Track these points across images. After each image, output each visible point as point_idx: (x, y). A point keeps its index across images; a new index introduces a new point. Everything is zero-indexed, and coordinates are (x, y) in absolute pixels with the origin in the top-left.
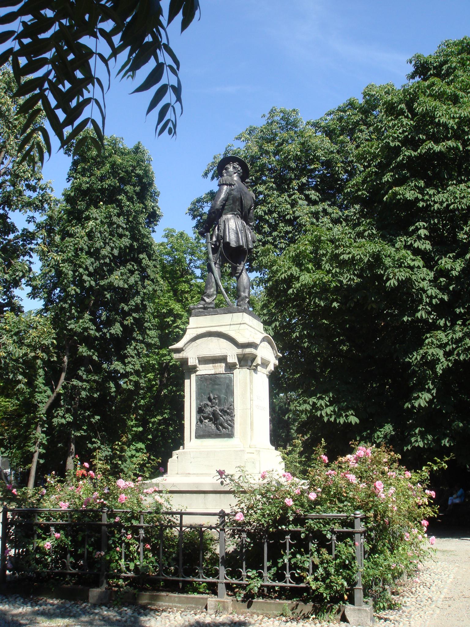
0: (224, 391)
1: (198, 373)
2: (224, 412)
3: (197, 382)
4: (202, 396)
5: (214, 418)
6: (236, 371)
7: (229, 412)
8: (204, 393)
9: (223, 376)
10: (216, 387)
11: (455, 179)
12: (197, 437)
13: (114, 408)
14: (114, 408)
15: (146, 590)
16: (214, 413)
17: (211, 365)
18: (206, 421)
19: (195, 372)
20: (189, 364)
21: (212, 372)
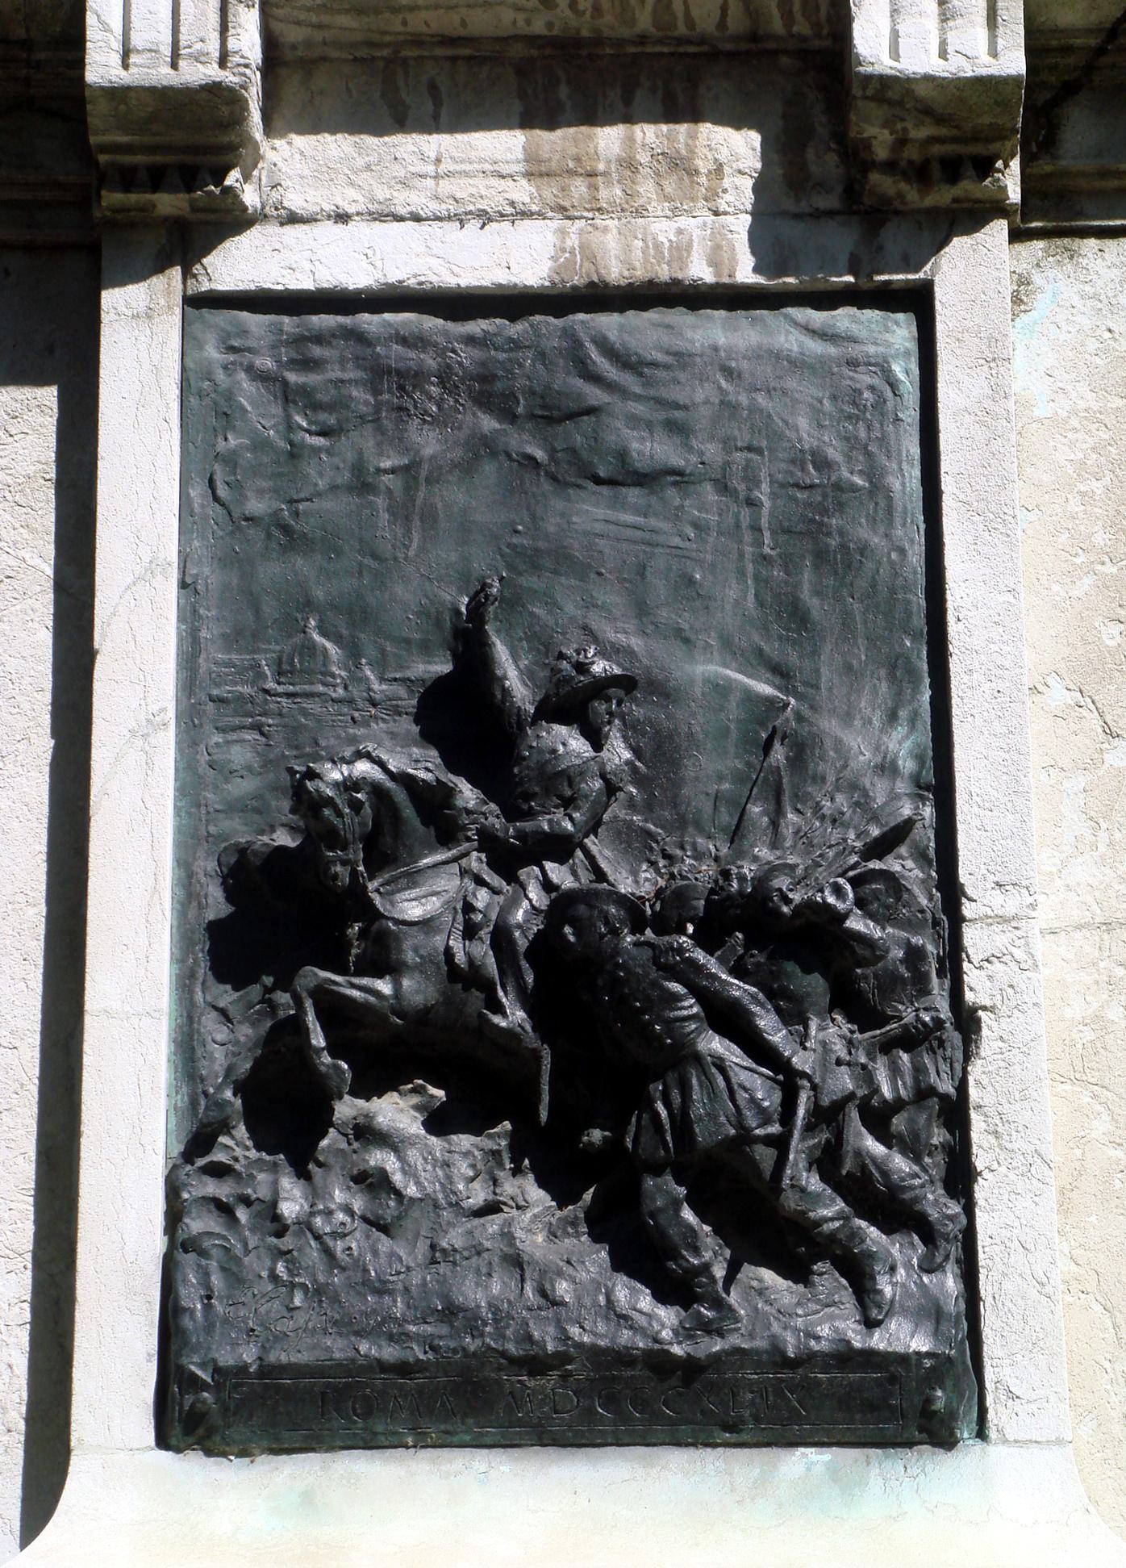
0: (735, 597)
1: (235, 265)
2: (798, 947)
3: (204, 409)
4: (299, 665)
5: (573, 1069)
6: (972, 271)
7: (877, 956)
8: (356, 621)
9: (712, 331)
10: (590, 513)
11: (526, 921)
12: (199, 1411)
13: (597, 1135)
14: (597, 1135)
15: (737, 38)
16: (569, 965)
17: (505, 145)
18: (395, 1111)
19: (188, 241)
20: (102, 65)
21: (525, 257)
